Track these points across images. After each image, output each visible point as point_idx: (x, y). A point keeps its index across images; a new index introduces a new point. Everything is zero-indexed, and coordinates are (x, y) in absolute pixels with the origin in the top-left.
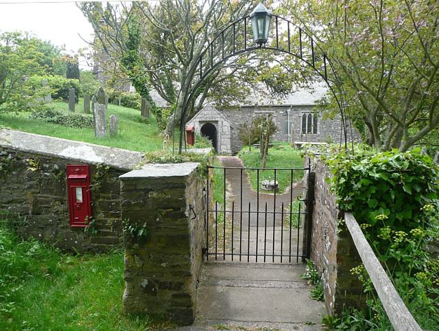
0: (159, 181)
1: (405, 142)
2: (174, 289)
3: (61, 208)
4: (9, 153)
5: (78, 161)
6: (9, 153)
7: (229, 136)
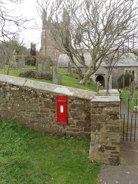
0: (108, 103)
1: (116, 155)
2: (112, 150)
3: (53, 115)
4: (32, 90)
5: (62, 94)
6: (32, 90)
7: (111, 82)
